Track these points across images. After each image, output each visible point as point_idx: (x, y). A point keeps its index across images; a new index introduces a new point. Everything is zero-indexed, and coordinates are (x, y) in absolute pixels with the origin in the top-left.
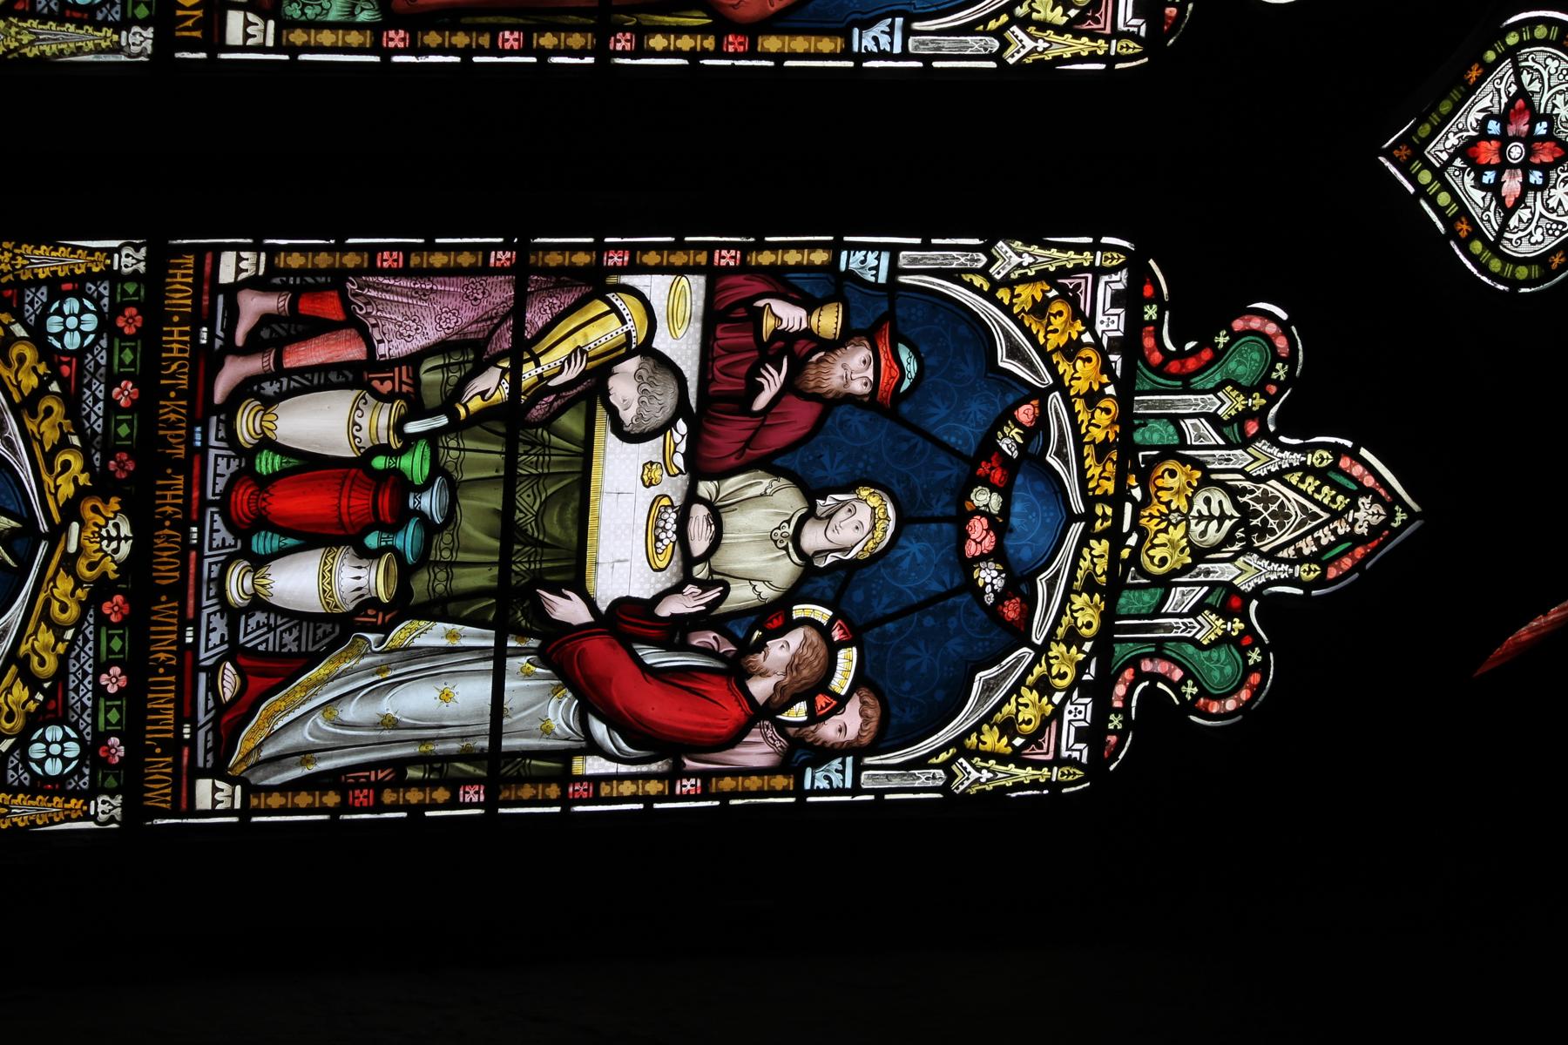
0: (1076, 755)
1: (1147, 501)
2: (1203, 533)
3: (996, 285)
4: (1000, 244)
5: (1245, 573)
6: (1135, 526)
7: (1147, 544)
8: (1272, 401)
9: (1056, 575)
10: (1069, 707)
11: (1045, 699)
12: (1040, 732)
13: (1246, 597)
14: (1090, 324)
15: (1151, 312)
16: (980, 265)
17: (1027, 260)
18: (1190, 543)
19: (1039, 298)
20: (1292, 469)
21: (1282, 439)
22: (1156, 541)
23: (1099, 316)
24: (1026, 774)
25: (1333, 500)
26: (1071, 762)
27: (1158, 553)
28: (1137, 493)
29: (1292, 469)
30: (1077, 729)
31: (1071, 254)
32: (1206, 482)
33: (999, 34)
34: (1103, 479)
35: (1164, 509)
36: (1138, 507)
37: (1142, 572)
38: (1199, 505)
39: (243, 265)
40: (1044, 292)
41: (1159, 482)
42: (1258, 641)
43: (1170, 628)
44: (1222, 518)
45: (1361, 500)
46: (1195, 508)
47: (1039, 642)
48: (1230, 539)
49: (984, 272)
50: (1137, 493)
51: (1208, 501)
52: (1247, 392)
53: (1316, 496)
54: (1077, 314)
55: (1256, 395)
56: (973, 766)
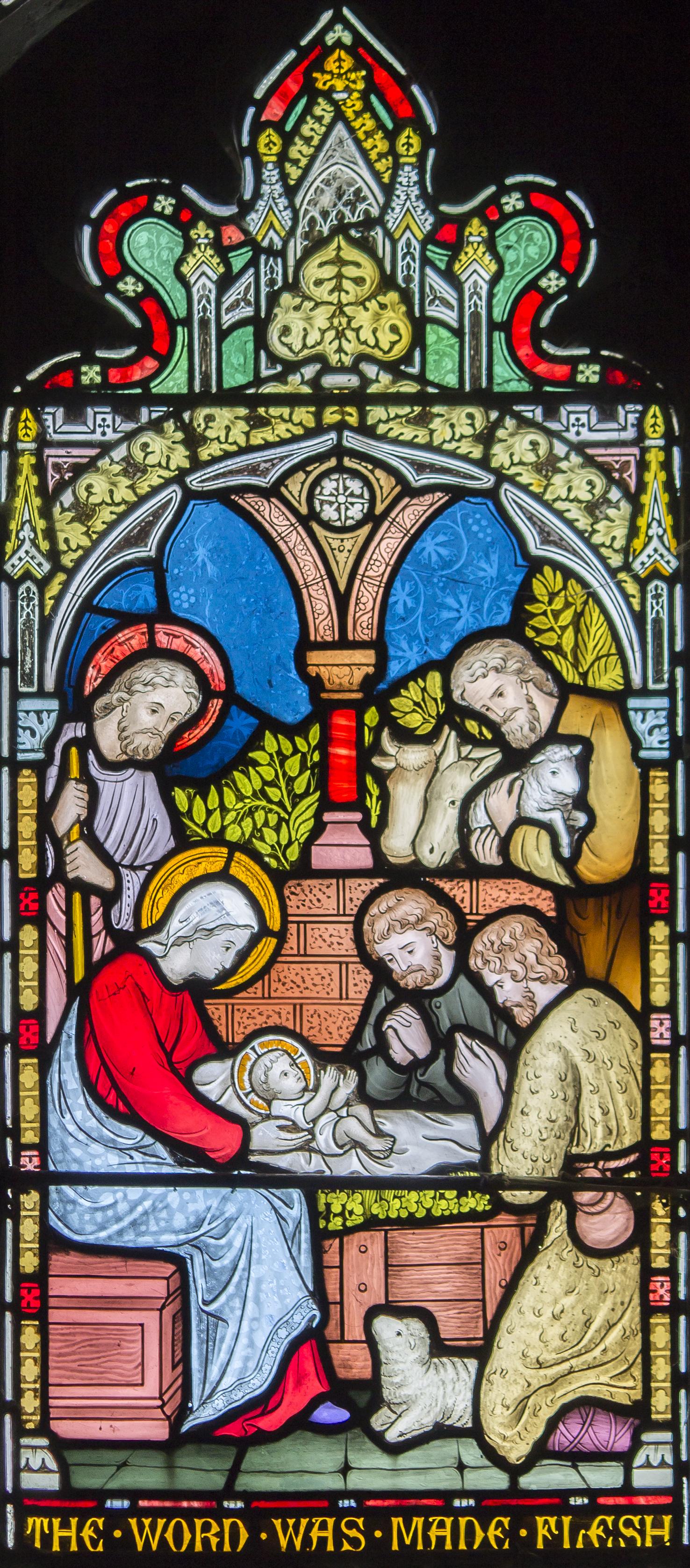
0: (632, 418)
1: (320, 358)
2: (359, 281)
3: (57, 567)
4: (8, 567)
5: (410, 217)
6: (354, 369)
7: (378, 354)
8: (199, 214)
9: (413, 463)
10: (571, 436)
11: (563, 465)
12: (605, 470)
13: (442, 220)
14: (106, 448)
15: (91, 374)
16: (34, 589)
17: (26, 533)
18: (372, 296)
19: (70, 515)
20: (284, 177)
21: (247, 196)
22: (372, 342)
23: (97, 437)
24: (655, 479)
25: (319, 119)
26: (640, 425)
27: (386, 338)
28: (309, 371)
29: (284, 177)
30: (599, 421)
31: (21, 481)
32: (293, 286)
33: (642, 583)
34: (284, 422)
35: (331, 334)
36: (327, 368)
37: (407, 359)
38: (322, 293)
39: (36, 1464)
40: (63, 510)
41: (297, 346)
42: (494, 201)
43: (476, 315)
44: (339, 261)
45: (319, 85)
46: (326, 298)
47: (493, 479)
48: (366, 246)
49: (43, 584)
50: (309, 371)
51: (319, 283)
52: (189, 245)
53: (315, 142)
54: (91, 465)
55: (192, 233)
56: (646, 545)
